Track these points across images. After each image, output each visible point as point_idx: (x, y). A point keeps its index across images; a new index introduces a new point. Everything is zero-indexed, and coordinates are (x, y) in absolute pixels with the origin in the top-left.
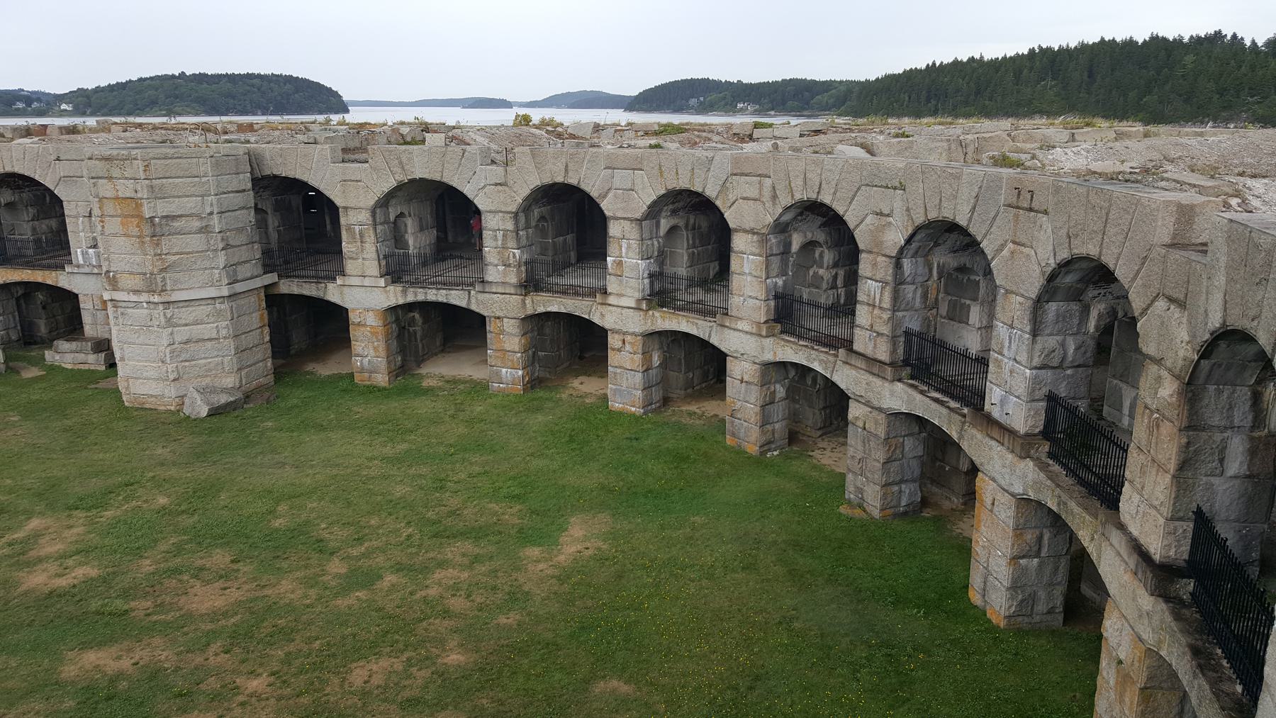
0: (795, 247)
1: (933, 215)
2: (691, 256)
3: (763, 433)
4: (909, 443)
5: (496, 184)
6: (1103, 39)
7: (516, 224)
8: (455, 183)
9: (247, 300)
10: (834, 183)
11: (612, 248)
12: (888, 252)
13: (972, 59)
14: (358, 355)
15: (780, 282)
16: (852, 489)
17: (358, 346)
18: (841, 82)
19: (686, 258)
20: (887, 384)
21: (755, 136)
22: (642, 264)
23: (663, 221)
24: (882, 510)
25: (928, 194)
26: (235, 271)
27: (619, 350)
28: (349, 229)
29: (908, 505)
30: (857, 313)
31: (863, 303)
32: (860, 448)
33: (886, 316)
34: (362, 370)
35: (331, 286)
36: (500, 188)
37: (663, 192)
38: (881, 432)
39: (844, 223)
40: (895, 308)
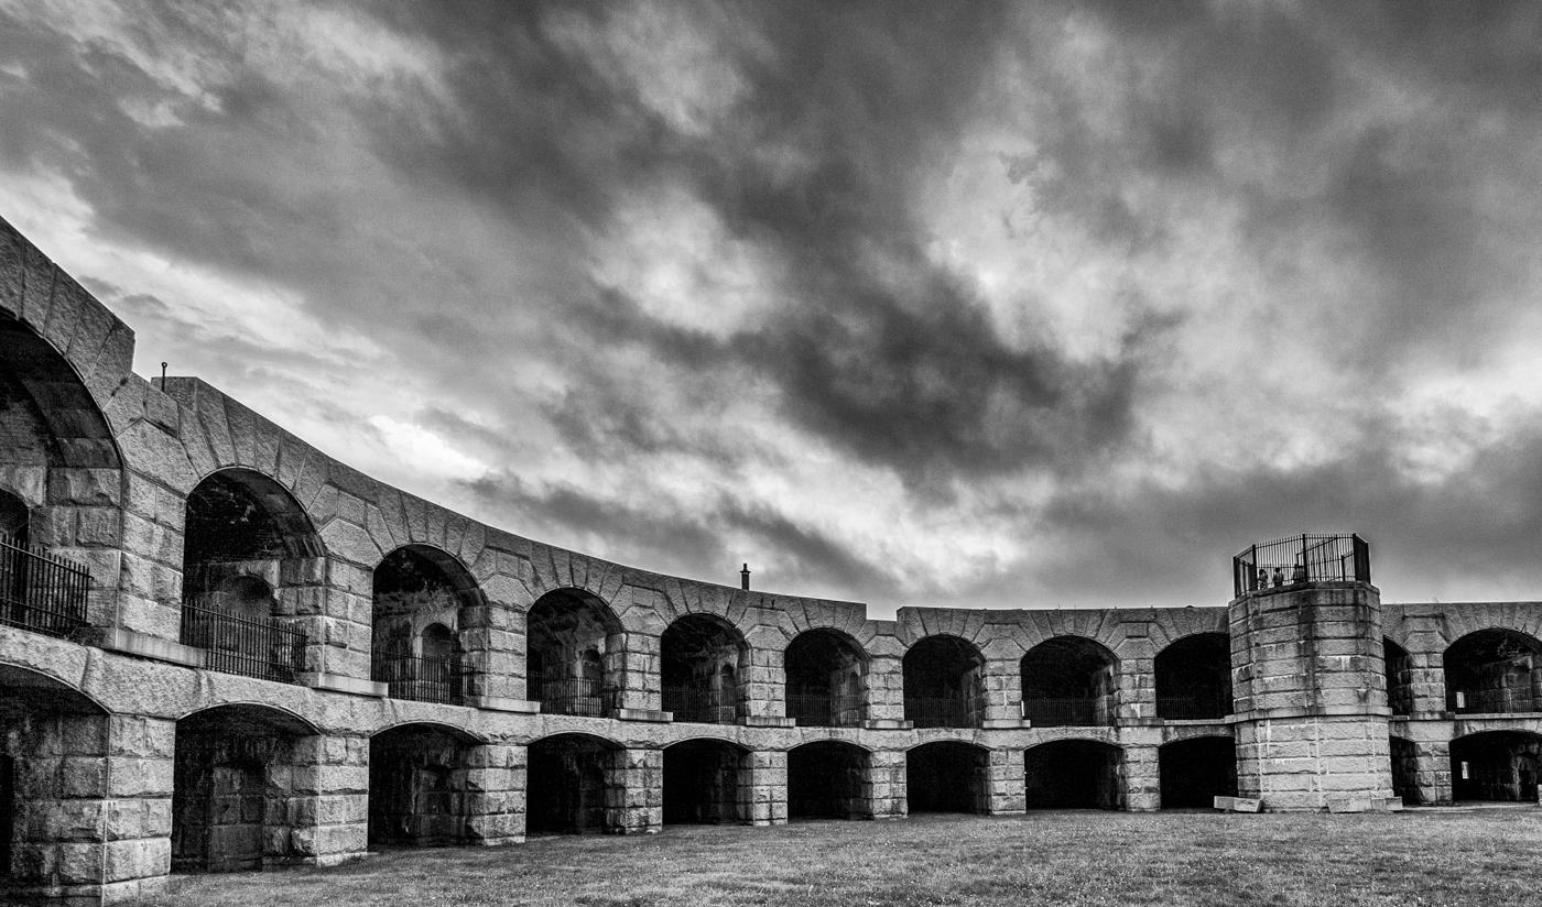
31: (632, 671)
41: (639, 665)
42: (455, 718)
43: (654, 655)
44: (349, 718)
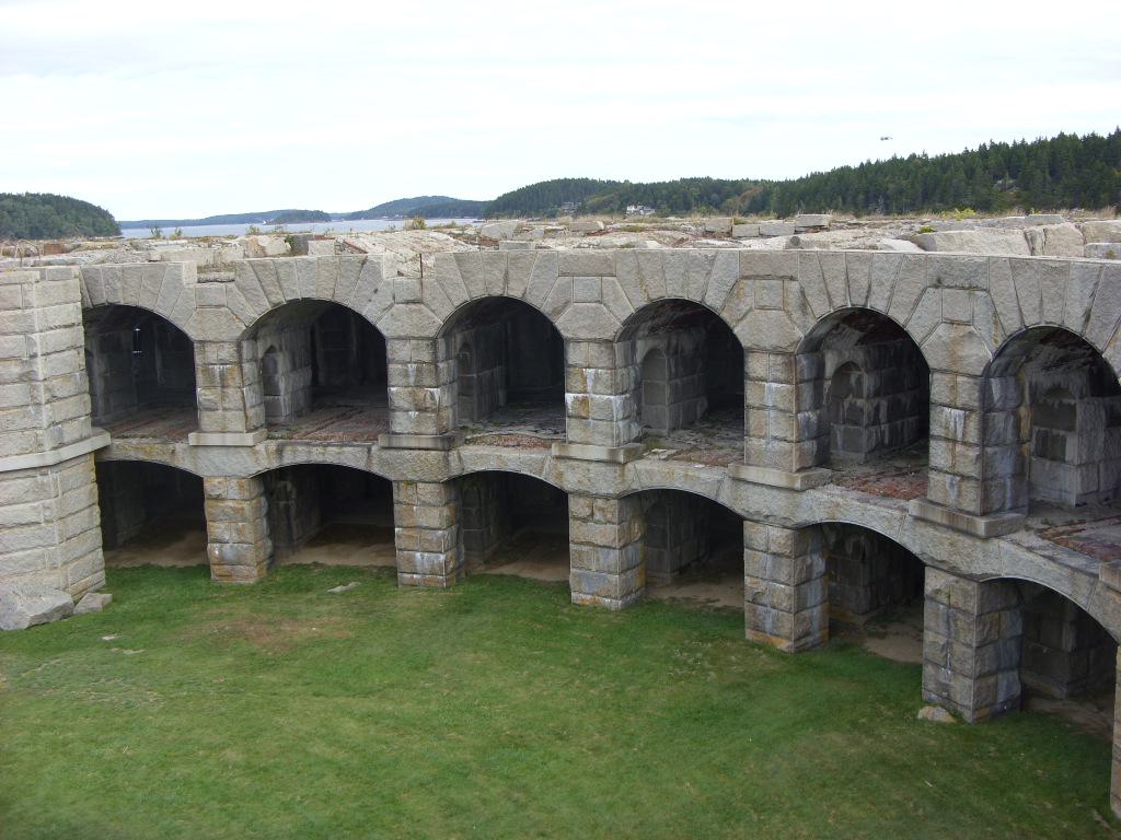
0: (829, 370)
1: (1032, 320)
2: (675, 389)
3: (798, 622)
4: (1007, 617)
5: (407, 302)
6: (1062, 135)
7: (435, 353)
8: (350, 302)
9: (73, 469)
10: (888, 285)
11: (572, 381)
12: (971, 370)
13: (913, 157)
14: (216, 541)
15: (813, 416)
16: (931, 686)
17: (216, 529)
18: (756, 182)
19: (668, 391)
20: (978, 543)
21: (735, 234)
22: (617, 400)
23: (640, 344)
24: (976, 709)
25: (1023, 294)
26: (61, 432)
27: (585, 520)
28: (207, 371)
29: (1004, 703)
30: (932, 451)
31: (939, 438)
32: (943, 629)
33: (973, 453)
34: (222, 561)
35: (179, 446)
36: (413, 306)
37: (643, 303)
38: (973, 606)
39: (906, 335)
40: (984, 442)
41: (947, 428)
42: (704, 487)
43: (972, 411)
44: (586, 481)
